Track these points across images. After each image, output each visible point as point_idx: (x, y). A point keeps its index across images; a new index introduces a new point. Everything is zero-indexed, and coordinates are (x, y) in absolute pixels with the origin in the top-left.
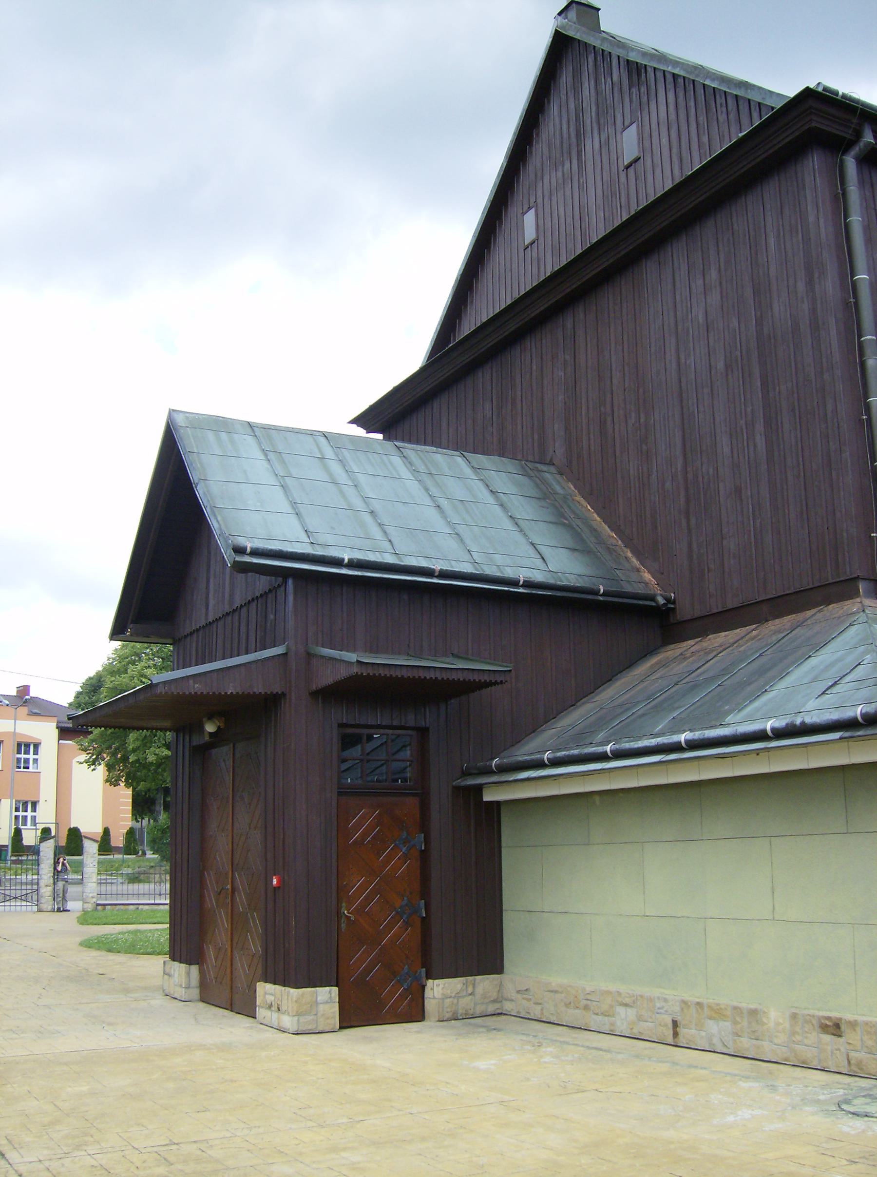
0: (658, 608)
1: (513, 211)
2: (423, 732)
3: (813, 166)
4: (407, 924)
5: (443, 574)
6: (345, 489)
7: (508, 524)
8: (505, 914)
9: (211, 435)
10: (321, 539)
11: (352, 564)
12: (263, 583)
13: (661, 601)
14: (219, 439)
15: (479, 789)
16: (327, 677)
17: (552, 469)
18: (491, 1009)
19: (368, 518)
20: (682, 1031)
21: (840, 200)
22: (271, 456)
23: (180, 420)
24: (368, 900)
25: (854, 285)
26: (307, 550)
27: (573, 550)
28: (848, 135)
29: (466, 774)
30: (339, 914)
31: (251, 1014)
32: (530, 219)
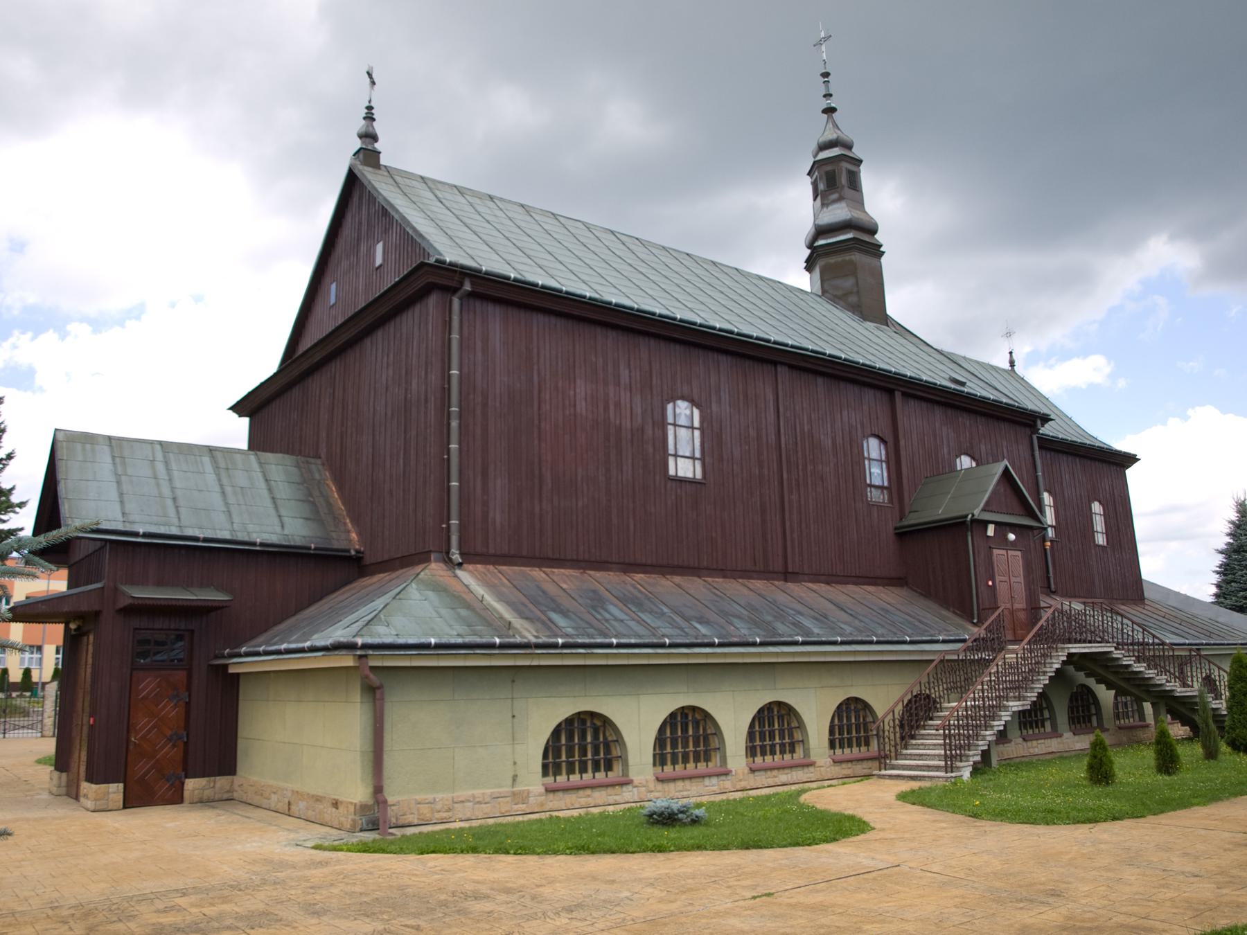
0: (350, 557)
1: (327, 279)
2: (192, 631)
3: (433, 300)
4: (174, 746)
5: (206, 540)
6: (162, 482)
7: (268, 503)
8: (239, 741)
9: (79, 447)
10: (131, 518)
11: (145, 535)
12: (99, 544)
13: (353, 553)
14: (84, 449)
15: (226, 667)
16: (123, 602)
17: (319, 462)
18: (225, 796)
19: (170, 503)
20: (293, 807)
21: (447, 325)
22: (118, 460)
23: (60, 437)
24: (149, 731)
25: (449, 376)
26: (120, 527)
27: (307, 519)
28: (454, 284)
29: (216, 657)
30: (128, 740)
31: (77, 798)
32: (334, 286)
